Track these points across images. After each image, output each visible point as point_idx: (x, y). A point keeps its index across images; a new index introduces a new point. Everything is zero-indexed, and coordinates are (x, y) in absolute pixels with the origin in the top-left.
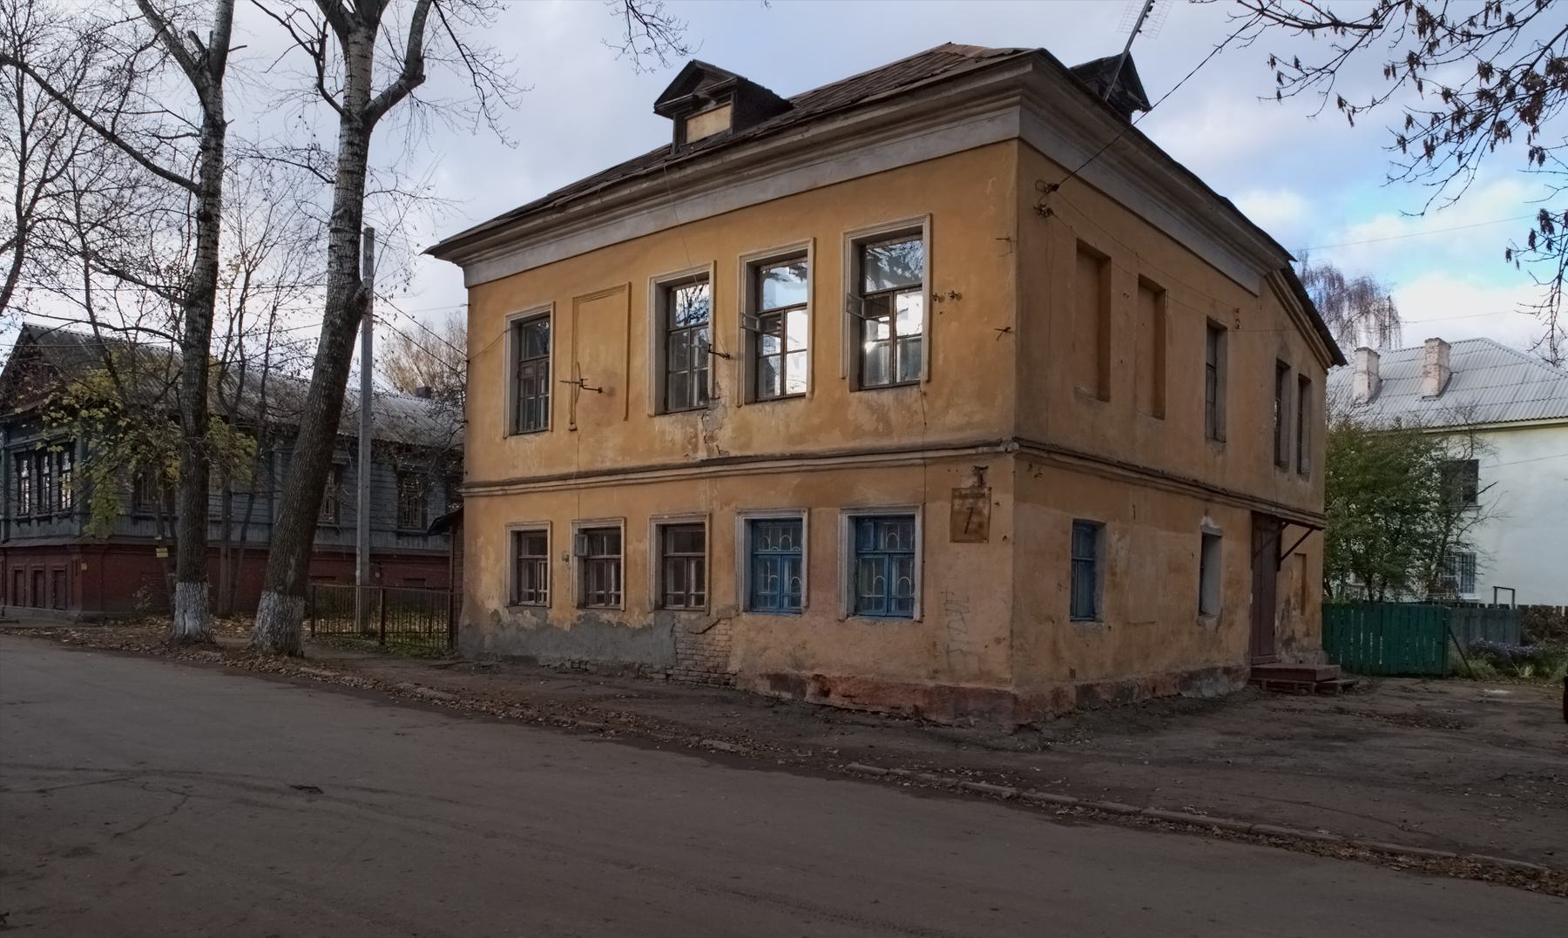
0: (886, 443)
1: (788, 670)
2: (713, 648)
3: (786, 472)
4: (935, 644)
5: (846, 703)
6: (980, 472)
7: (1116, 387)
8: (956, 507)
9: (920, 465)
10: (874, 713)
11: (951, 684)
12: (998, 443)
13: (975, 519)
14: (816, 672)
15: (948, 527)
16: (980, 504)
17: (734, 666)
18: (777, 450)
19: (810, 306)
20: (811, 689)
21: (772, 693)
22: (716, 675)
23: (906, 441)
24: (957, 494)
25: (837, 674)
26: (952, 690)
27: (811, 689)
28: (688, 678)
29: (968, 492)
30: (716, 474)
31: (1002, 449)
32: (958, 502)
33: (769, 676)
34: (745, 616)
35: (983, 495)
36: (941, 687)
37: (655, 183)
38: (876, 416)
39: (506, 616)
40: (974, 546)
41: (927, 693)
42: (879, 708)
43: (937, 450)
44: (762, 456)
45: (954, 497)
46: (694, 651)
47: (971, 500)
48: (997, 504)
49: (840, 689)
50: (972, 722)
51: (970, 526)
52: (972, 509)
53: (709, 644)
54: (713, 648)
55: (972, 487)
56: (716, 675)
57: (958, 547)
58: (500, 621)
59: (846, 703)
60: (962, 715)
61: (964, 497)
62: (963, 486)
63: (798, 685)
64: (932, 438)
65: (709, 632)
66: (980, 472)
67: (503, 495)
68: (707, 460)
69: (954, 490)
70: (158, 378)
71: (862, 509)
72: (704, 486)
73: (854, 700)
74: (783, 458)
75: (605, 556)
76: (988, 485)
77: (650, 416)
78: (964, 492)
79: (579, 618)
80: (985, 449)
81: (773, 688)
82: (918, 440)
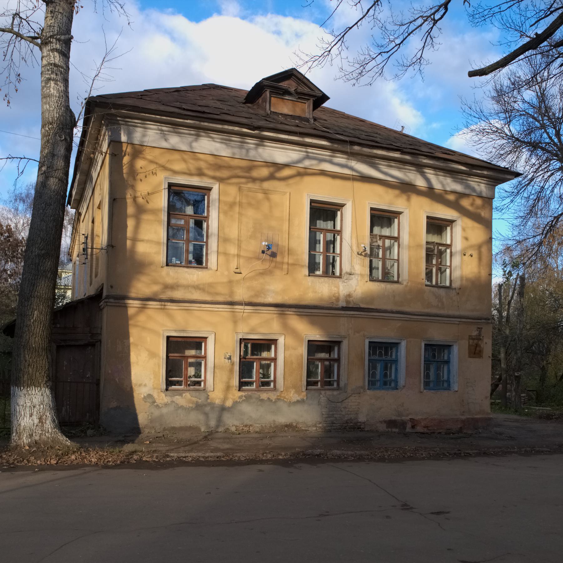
0: (442, 312)
1: (394, 418)
2: (347, 410)
3: (396, 320)
4: (463, 401)
5: (425, 430)
6: (480, 329)
7: (427, 287)
8: (470, 343)
9: (457, 324)
10: (438, 433)
11: (471, 417)
12: (489, 319)
13: (478, 349)
14: (410, 417)
15: (467, 352)
16: (480, 343)
17: (362, 418)
18: (389, 307)
19: (334, 230)
20: (409, 425)
21: (387, 430)
22: (351, 424)
23: (451, 313)
24: (471, 338)
25: (420, 417)
26: (473, 419)
27: (409, 425)
28: (333, 428)
29: (475, 337)
30: (354, 316)
31: (490, 321)
32: (471, 341)
33: (385, 422)
34: (368, 392)
35: (481, 339)
36: (468, 418)
37: (253, 132)
38: (437, 299)
39: (162, 398)
40: (477, 359)
41: (463, 421)
42: (441, 431)
43: (466, 319)
44: (380, 310)
45: (469, 339)
46: (335, 412)
47: (476, 341)
48: (486, 343)
49: (422, 424)
50: (481, 431)
51: (476, 351)
52: (477, 344)
53: (345, 408)
54: (347, 410)
55: (476, 336)
56: (351, 424)
57: (471, 360)
58: (154, 402)
59: (425, 430)
60: (476, 429)
61: (473, 339)
62: (473, 335)
63: (403, 424)
64: (462, 313)
65: (345, 401)
66: (480, 329)
67: (161, 309)
68: (346, 307)
69: (470, 336)
70: (434, 18)
71: (432, 341)
72: (343, 321)
73: (429, 428)
74: (392, 312)
75: (388, 386)
76: (482, 335)
77: (305, 276)
78: (473, 337)
79: (240, 397)
80: (484, 321)
81: (387, 427)
82: (457, 313)
